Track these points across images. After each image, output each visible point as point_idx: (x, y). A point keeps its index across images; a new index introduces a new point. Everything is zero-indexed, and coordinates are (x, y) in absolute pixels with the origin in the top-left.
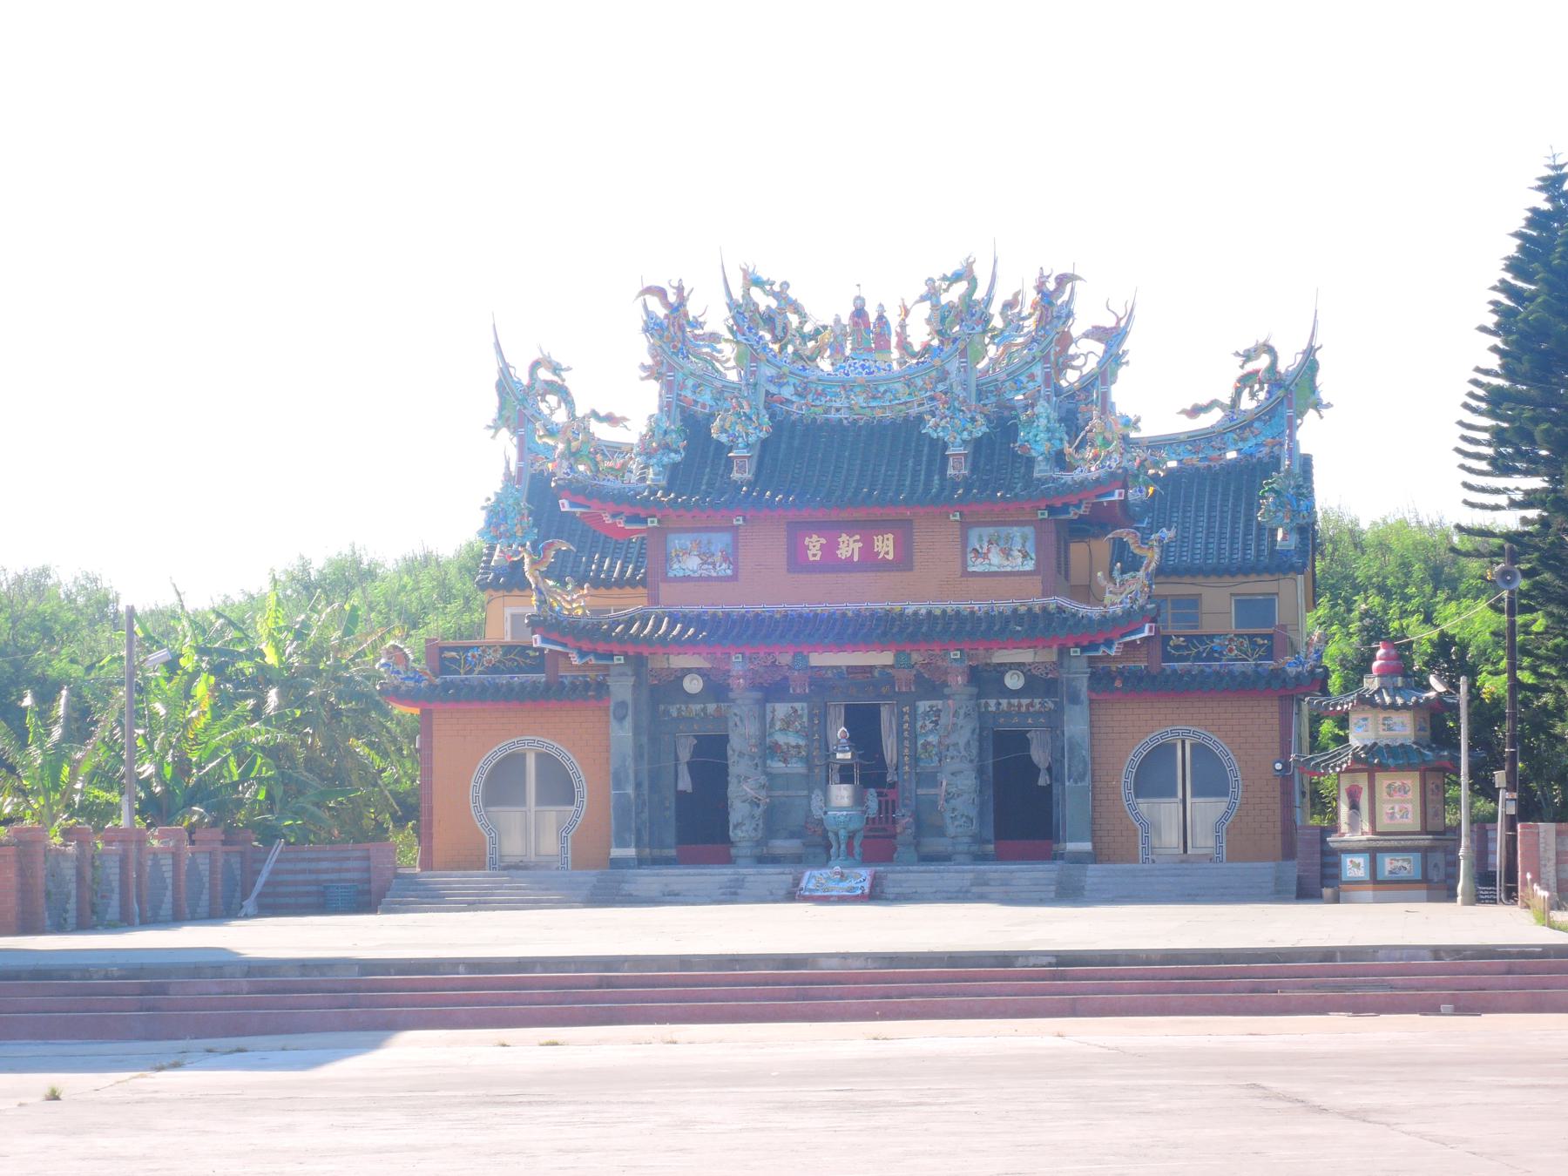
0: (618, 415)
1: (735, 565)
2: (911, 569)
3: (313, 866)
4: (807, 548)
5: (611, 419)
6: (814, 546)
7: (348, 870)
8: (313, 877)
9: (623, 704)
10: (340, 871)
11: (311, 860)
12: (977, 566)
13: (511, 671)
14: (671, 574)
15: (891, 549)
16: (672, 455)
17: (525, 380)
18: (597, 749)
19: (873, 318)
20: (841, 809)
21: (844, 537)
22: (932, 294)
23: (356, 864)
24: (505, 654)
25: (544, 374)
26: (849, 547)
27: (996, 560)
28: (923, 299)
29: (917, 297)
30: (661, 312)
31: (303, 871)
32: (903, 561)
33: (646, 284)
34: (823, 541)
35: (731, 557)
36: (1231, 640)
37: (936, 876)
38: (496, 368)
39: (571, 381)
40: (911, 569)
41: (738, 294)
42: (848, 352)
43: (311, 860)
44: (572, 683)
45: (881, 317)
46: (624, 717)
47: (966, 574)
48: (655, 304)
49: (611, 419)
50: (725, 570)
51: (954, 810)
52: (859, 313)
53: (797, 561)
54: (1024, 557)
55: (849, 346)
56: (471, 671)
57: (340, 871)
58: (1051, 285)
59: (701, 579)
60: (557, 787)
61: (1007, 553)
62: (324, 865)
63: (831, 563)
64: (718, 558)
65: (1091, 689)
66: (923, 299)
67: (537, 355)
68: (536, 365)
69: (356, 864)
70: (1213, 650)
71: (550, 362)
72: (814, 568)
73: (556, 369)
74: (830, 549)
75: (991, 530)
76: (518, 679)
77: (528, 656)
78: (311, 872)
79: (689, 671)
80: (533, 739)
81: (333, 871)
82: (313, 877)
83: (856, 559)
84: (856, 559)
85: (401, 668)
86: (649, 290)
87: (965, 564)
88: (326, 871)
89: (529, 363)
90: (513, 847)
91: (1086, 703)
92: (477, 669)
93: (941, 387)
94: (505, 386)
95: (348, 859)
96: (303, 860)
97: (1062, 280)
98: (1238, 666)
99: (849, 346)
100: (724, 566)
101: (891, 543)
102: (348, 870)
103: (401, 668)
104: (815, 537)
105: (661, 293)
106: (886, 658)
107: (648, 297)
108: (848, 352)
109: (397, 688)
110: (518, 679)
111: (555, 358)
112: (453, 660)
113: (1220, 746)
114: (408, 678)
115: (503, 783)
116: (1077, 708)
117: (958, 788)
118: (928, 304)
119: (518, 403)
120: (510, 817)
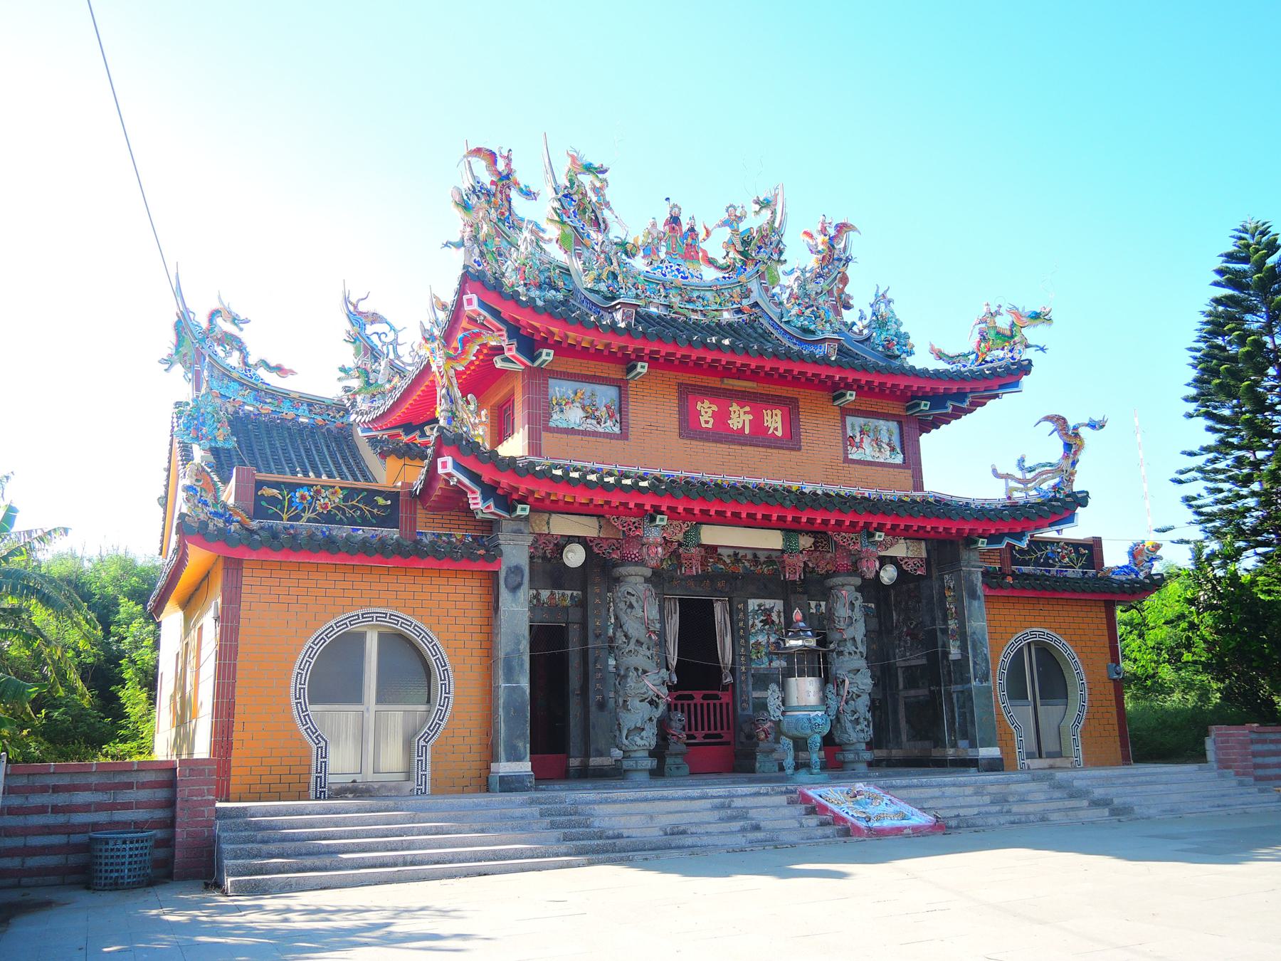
0: (287, 367)
1: (623, 423)
2: (799, 449)
3: (61, 799)
4: (699, 413)
5: (279, 370)
6: (706, 411)
7: (127, 806)
8: (61, 819)
9: (517, 570)
10: (113, 807)
11: (56, 789)
12: (855, 454)
13: (352, 522)
14: (551, 424)
15: (779, 425)
16: (553, 292)
17: (204, 325)
18: (467, 633)
19: (685, 228)
20: (805, 708)
21: (735, 407)
22: (733, 220)
23: (144, 795)
24: (345, 499)
25: (224, 325)
26: (740, 418)
27: (867, 452)
28: (724, 224)
29: (718, 222)
30: (486, 178)
31: (41, 810)
32: (791, 440)
33: (472, 147)
34: (715, 408)
35: (621, 411)
36: (1063, 548)
37: (936, 792)
38: (175, 309)
39: (246, 335)
40: (799, 449)
41: (563, 181)
42: (663, 255)
43: (56, 789)
44: (433, 543)
45: (692, 230)
46: (519, 586)
47: (847, 460)
48: (480, 166)
49: (279, 370)
50: (610, 427)
51: (854, 712)
52: (674, 220)
53: (689, 428)
54: (893, 449)
55: (663, 250)
56: (297, 517)
57: (113, 807)
58: (832, 232)
59: (585, 433)
60: (409, 666)
61: (877, 442)
62: (82, 798)
63: (722, 434)
64: (602, 412)
65: (985, 584)
66: (724, 224)
67: (216, 305)
68: (214, 314)
69: (144, 795)
70: (1048, 558)
71: (230, 313)
72: (705, 436)
73: (235, 320)
74: (721, 417)
75: (861, 421)
76: (362, 532)
77: (376, 505)
78: (56, 809)
79: (571, 539)
80: (376, 606)
81: (100, 807)
82: (61, 819)
83: (747, 431)
84: (747, 431)
85: (210, 500)
86: (478, 151)
87: (846, 452)
88: (86, 808)
89: (207, 312)
90: (342, 763)
91: (982, 598)
92: (306, 515)
93: (745, 302)
94: (182, 326)
95: (129, 786)
96: (44, 789)
97: (842, 228)
98: (1070, 573)
99: (663, 250)
100: (609, 423)
101: (779, 419)
102: (127, 806)
103: (210, 500)
104: (707, 403)
105: (492, 157)
106: (771, 540)
107: (474, 160)
108: (663, 255)
109: (204, 525)
110: (362, 532)
111: (235, 310)
112: (273, 500)
113: (1066, 649)
114: (216, 514)
115: (335, 677)
116: (976, 603)
117: (642, 685)
118: (728, 230)
119: (197, 343)
120: (338, 719)
